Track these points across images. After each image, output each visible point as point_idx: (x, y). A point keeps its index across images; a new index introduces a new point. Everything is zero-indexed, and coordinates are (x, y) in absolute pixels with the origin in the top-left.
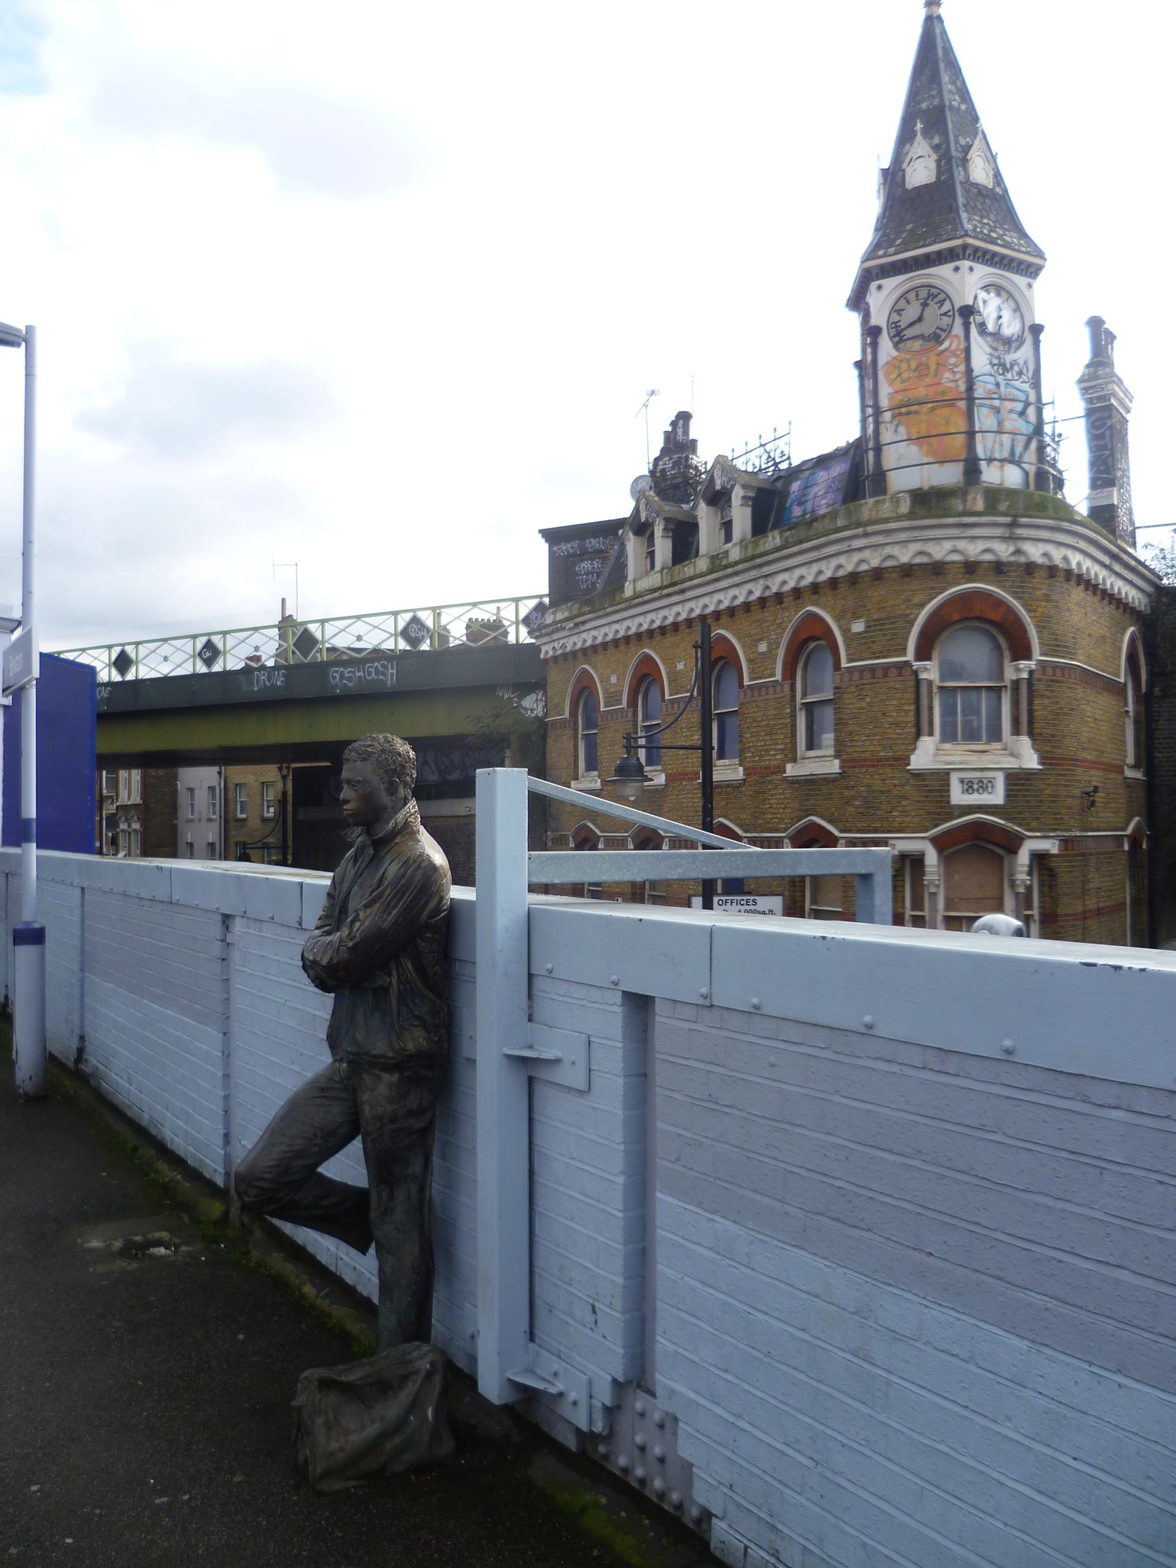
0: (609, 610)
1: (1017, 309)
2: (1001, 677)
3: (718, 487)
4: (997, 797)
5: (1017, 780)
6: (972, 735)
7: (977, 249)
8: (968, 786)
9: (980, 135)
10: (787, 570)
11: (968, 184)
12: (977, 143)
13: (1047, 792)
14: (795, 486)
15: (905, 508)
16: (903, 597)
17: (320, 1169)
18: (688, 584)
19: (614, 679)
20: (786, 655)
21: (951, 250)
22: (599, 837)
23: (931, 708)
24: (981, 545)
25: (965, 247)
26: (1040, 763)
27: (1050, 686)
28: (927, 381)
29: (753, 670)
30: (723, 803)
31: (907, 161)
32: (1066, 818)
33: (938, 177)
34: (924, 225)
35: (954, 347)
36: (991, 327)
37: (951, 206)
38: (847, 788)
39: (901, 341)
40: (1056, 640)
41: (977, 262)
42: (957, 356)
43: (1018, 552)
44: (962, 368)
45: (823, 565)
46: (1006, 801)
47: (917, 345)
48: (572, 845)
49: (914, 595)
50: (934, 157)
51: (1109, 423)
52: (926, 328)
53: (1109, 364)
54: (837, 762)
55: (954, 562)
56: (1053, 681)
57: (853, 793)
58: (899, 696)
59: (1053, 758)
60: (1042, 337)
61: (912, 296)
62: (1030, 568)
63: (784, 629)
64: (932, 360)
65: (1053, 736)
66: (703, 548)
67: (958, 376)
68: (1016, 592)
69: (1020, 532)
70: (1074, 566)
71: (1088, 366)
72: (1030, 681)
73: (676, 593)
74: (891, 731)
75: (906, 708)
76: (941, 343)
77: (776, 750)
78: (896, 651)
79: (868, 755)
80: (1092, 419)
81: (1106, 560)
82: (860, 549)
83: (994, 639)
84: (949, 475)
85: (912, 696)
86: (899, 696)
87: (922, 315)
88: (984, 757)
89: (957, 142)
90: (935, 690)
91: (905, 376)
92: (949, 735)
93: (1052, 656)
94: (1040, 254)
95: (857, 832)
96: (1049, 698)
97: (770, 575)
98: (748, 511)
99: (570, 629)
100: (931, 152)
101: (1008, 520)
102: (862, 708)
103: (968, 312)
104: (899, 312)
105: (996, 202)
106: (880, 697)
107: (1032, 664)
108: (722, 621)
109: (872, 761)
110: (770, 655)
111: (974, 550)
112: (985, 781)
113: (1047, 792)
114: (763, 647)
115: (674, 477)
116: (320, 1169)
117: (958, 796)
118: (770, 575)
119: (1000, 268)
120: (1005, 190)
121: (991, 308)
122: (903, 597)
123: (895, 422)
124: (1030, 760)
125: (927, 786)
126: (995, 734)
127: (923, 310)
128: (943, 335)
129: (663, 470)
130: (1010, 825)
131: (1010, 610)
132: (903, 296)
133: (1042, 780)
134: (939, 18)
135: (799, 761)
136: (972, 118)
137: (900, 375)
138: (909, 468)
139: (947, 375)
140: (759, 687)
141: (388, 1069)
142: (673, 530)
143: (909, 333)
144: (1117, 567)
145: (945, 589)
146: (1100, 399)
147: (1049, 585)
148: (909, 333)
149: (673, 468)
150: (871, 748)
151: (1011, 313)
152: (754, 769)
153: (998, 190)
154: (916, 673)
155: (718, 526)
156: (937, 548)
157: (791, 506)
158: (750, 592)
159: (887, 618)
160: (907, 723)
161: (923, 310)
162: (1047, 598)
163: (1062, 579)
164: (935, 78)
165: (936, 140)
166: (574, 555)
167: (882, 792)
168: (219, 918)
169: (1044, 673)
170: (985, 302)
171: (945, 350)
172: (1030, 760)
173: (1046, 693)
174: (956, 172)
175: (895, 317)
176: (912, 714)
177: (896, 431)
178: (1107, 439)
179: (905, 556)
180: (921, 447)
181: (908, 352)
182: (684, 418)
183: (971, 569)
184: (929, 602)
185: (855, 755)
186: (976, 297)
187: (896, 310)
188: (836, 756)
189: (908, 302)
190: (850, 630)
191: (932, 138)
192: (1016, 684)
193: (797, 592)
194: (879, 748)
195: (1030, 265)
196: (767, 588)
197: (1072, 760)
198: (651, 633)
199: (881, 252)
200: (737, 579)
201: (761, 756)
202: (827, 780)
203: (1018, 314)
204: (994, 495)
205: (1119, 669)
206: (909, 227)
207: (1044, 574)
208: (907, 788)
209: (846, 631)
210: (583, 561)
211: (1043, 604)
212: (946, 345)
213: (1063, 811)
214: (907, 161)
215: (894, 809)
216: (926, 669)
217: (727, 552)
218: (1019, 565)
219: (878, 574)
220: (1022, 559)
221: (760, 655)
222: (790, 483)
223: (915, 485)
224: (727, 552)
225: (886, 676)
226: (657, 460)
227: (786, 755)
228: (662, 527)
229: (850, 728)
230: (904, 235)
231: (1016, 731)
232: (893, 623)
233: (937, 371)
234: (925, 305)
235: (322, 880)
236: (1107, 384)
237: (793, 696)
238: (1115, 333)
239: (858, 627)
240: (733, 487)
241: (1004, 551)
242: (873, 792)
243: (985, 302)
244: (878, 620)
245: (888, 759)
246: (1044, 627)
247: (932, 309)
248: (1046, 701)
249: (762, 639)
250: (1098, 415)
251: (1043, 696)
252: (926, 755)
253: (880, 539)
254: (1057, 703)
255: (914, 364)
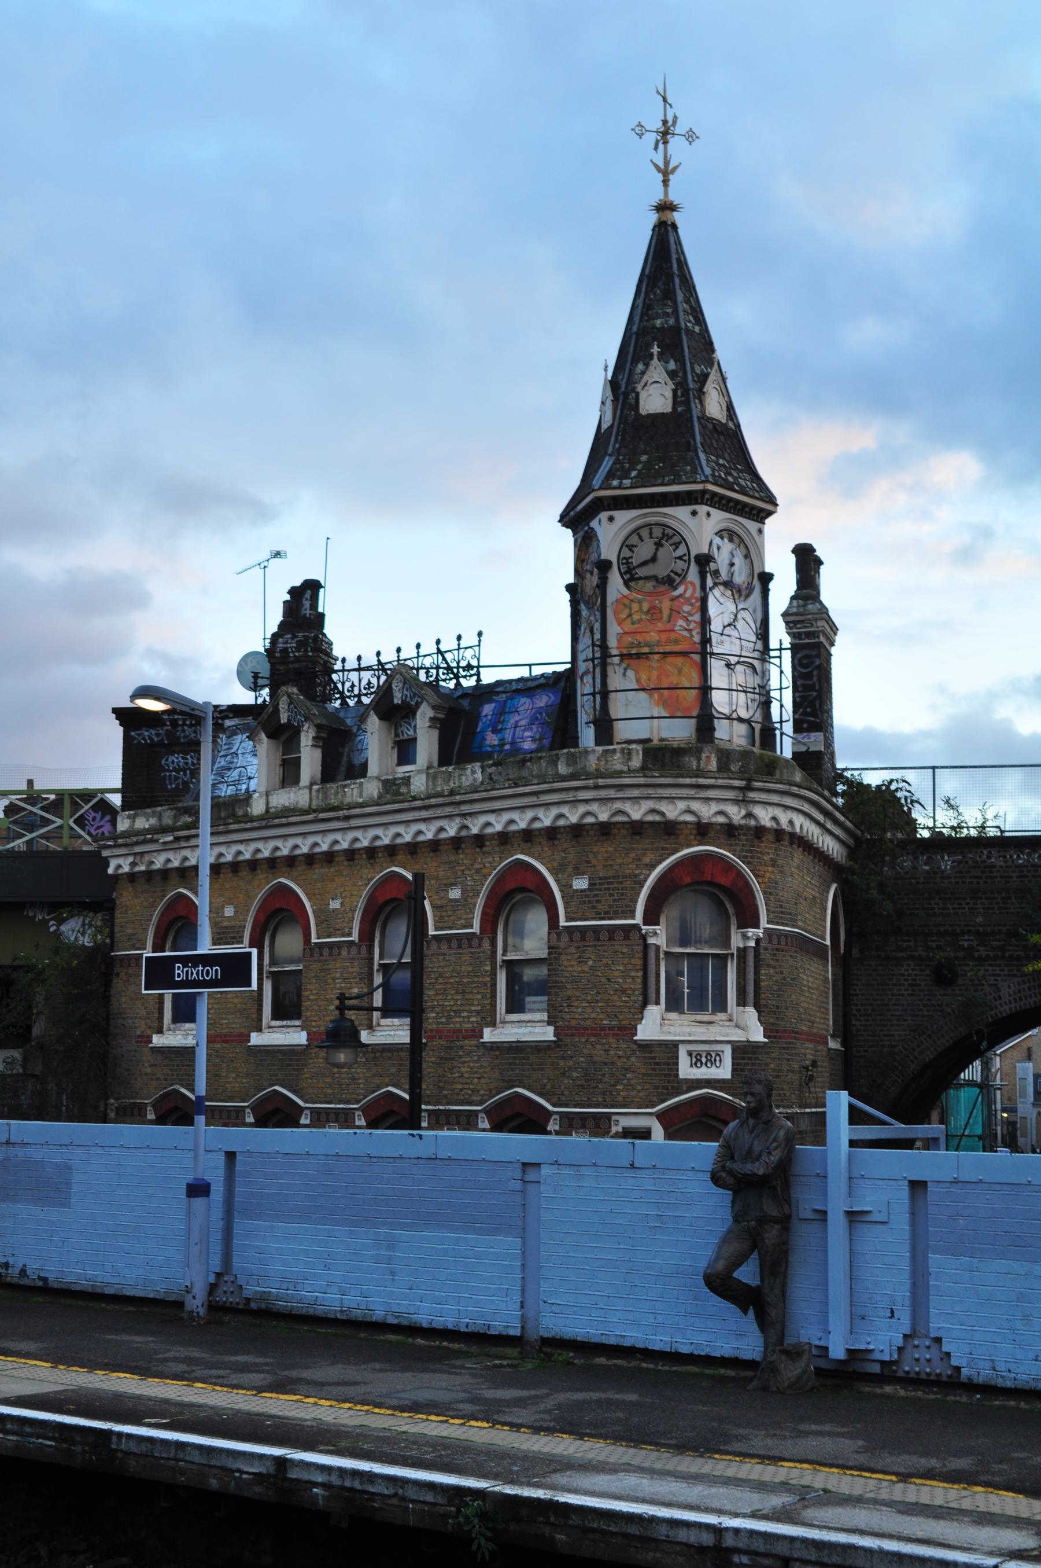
0: (232, 827)
1: (747, 556)
2: (727, 944)
3: (397, 700)
4: (724, 1071)
5: (743, 1052)
6: (698, 1004)
7: (714, 494)
8: (697, 1060)
9: (716, 366)
10: (493, 811)
11: (704, 418)
12: (713, 375)
13: (772, 1066)
14: (488, 709)
15: (636, 762)
16: (632, 855)
17: (735, 1275)
18: (358, 811)
19: (229, 911)
20: (486, 905)
21: (689, 493)
22: (550, 1114)
23: (658, 975)
24: (714, 807)
25: (704, 492)
26: (765, 1036)
27: (775, 955)
28: (660, 626)
29: (442, 917)
30: (393, 1070)
31: (642, 384)
32: (788, 1094)
33: (674, 407)
34: (660, 460)
35: (688, 594)
36: (724, 576)
37: (689, 443)
38: (563, 1058)
39: (633, 579)
40: (781, 906)
41: (714, 507)
42: (692, 605)
43: (749, 815)
44: (697, 617)
45: (540, 813)
46: (732, 1075)
47: (649, 586)
48: (151, 1116)
49: (644, 854)
50: (671, 386)
51: (817, 662)
52: (660, 570)
53: (816, 597)
54: (551, 1029)
55: (686, 823)
56: (777, 950)
57: (571, 1063)
58: (626, 961)
59: (777, 1031)
60: (772, 585)
61: (645, 533)
62: (760, 831)
63: (485, 877)
64: (666, 606)
65: (777, 1007)
66: (373, 769)
67: (692, 625)
68: (746, 857)
69: (751, 795)
70: (798, 830)
71: (793, 598)
72: (756, 949)
73: (338, 819)
74: (616, 998)
75: (633, 974)
76: (675, 588)
77: (470, 1011)
78: (623, 912)
79: (588, 1022)
80: (799, 656)
81: (820, 817)
82: (587, 801)
83: (721, 905)
84: (679, 731)
85: (640, 962)
86: (626, 961)
87: (655, 554)
88: (712, 1029)
89: (693, 370)
90: (662, 956)
91: (635, 617)
92: (674, 1004)
93: (778, 924)
94: (772, 500)
95: (575, 1107)
96: (774, 967)
97: (470, 814)
98: (435, 734)
99: (164, 843)
100: (668, 379)
101: (741, 783)
102: (583, 972)
103: (704, 561)
104: (631, 548)
105: (729, 440)
106: (605, 961)
107: (760, 932)
108: (399, 857)
109: (593, 1029)
110: (465, 903)
111: (707, 812)
112: (714, 1055)
113: (772, 1066)
114: (455, 894)
115: (297, 659)
116: (735, 1275)
117: (686, 1070)
118: (470, 814)
119: (734, 513)
120: (738, 426)
121: (724, 553)
122: (632, 855)
123: (624, 665)
124: (757, 1034)
125: (654, 1058)
126: (721, 1006)
127: (657, 549)
128: (678, 579)
129: (285, 651)
130: (737, 1101)
131: (740, 875)
132: (636, 531)
133: (767, 1053)
134: (674, 227)
135: (498, 1025)
136: (708, 346)
137: (630, 615)
138: (641, 717)
139: (681, 622)
140: (448, 938)
141: (776, 1223)
142: (323, 739)
143: (641, 572)
144: (829, 825)
145: (678, 851)
146: (808, 635)
147: (776, 849)
148: (641, 572)
149: (298, 649)
150: (593, 1016)
151: (742, 558)
152: (438, 1031)
153: (731, 424)
154: (644, 938)
155: (390, 745)
156: (671, 807)
157: (483, 731)
158: (442, 829)
159: (614, 878)
160: (634, 990)
161: (657, 549)
162: (774, 863)
163: (786, 843)
164: (669, 294)
165: (672, 365)
166: (160, 744)
167: (606, 1064)
168: (520, 1165)
169: (770, 942)
170: (719, 548)
171: (680, 596)
172: (757, 1034)
173: (772, 962)
174: (693, 406)
175: (626, 553)
176: (639, 981)
177: (624, 675)
178: (815, 679)
179: (637, 813)
180: (651, 696)
181: (639, 592)
182: (312, 587)
183: (702, 831)
184: (660, 863)
185: (574, 1023)
186: (711, 543)
187: (627, 545)
188: (549, 1023)
189: (641, 538)
190: (571, 886)
191: (667, 362)
192: (743, 952)
193: (504, 838)
194: (601, 1016)
195: (761, 510)
196: (466, 827)
197: (793, 1032)
198: (291, 861)
199: (615, 483)
200: (424, 814)
201: (449, 1017)
202: (539, 1047)
203: (748, 560)
204: (725, 757)
205: (825, 932)
206: (644, 458)
207: (771, 837)
208: (633, 1059)
209: (565, 888)
210: (173, 753)
211: (770, 869)
212: (680, 590)
213: (785, 1087)
214: (642, 384)
215: (618, 1081)
216: (655, 934)
217: (407, 780)
218: (748, 828)
219: (605, 829)
220: (753, 823)
221: (456, 904)
222: (482, 704)
223: (644, 735)
224: (407, 780)
225: (611, 938)
226: (275, 637)
227: (484, 1018)
228: (312, 733)
229: (569, 993)
230: (639, 467)
231: (742, 1002)
232: (621, 883)
233: (670, 616)
234: (659, 545)
235: (717, 1144)
236: (816, 620)
237: (494, 952)
238: (823, 559)
239: (581, 884)
240: (418, 705)
241: (736, 814)
242: (594, 1063)
243: (719, 548)
244: (606, 878)
245: (612, 1028)
246: (771, 894)
247: (667, 549)
248: (772, 971)
249: (455, 885)
250: (806, 652)
251: (769, 966)
252: (653, 1025)
253: (612, 793)
254: (782, 972)
255: (646, 606)
